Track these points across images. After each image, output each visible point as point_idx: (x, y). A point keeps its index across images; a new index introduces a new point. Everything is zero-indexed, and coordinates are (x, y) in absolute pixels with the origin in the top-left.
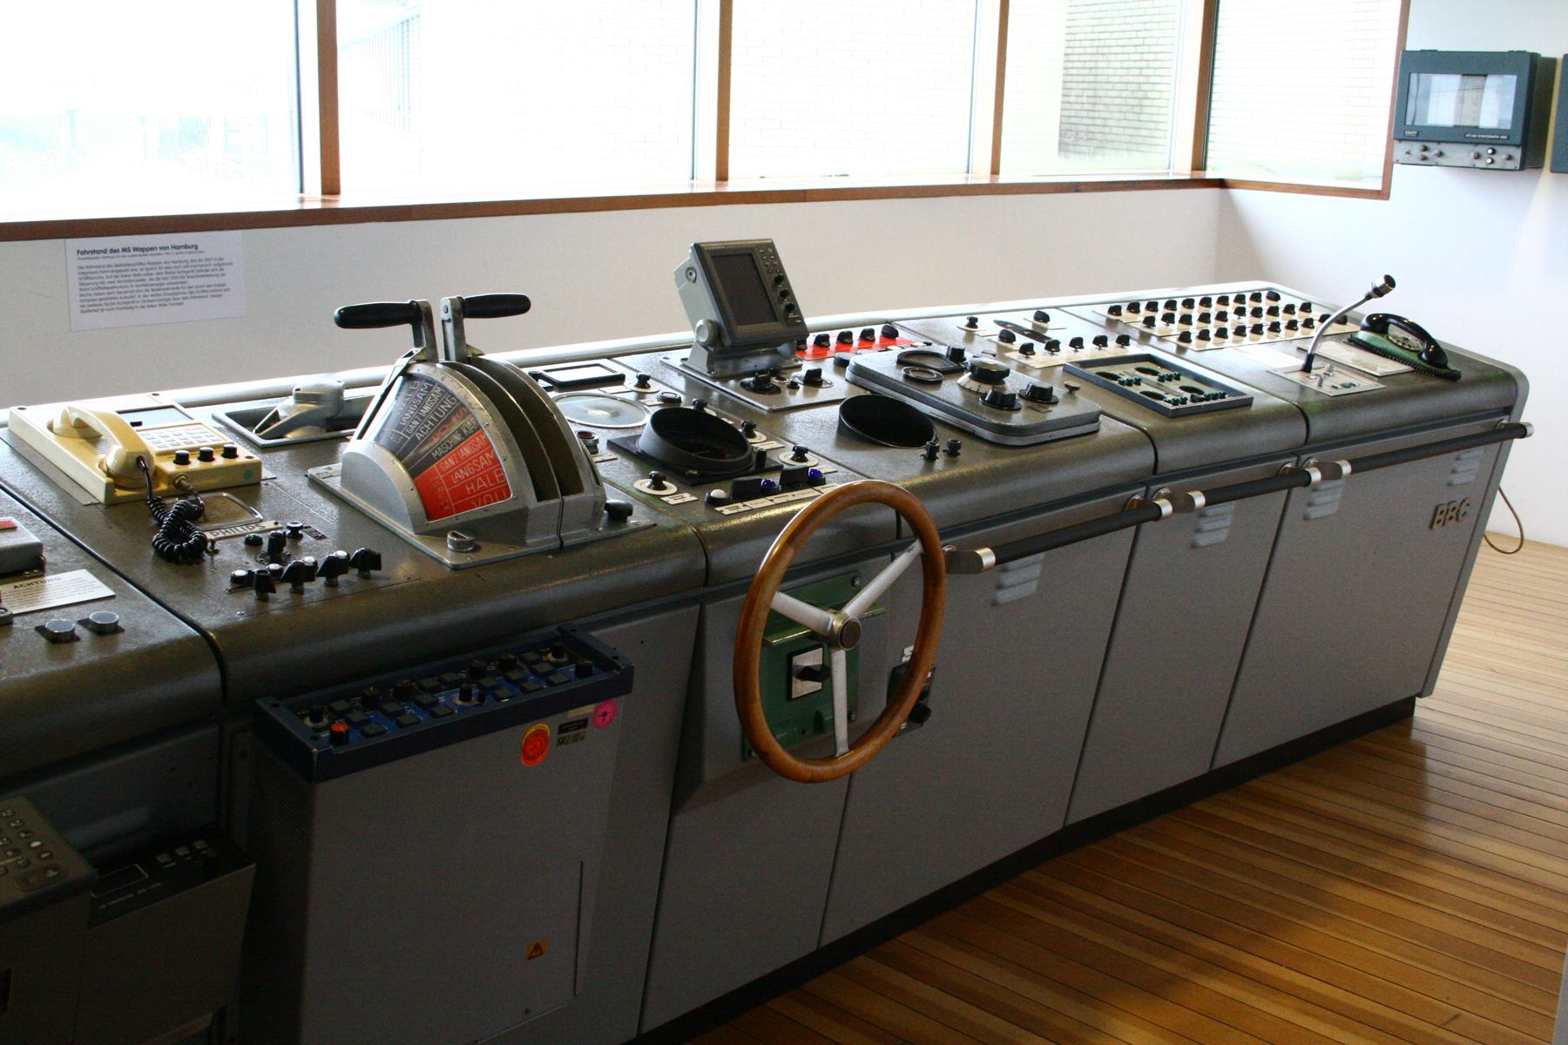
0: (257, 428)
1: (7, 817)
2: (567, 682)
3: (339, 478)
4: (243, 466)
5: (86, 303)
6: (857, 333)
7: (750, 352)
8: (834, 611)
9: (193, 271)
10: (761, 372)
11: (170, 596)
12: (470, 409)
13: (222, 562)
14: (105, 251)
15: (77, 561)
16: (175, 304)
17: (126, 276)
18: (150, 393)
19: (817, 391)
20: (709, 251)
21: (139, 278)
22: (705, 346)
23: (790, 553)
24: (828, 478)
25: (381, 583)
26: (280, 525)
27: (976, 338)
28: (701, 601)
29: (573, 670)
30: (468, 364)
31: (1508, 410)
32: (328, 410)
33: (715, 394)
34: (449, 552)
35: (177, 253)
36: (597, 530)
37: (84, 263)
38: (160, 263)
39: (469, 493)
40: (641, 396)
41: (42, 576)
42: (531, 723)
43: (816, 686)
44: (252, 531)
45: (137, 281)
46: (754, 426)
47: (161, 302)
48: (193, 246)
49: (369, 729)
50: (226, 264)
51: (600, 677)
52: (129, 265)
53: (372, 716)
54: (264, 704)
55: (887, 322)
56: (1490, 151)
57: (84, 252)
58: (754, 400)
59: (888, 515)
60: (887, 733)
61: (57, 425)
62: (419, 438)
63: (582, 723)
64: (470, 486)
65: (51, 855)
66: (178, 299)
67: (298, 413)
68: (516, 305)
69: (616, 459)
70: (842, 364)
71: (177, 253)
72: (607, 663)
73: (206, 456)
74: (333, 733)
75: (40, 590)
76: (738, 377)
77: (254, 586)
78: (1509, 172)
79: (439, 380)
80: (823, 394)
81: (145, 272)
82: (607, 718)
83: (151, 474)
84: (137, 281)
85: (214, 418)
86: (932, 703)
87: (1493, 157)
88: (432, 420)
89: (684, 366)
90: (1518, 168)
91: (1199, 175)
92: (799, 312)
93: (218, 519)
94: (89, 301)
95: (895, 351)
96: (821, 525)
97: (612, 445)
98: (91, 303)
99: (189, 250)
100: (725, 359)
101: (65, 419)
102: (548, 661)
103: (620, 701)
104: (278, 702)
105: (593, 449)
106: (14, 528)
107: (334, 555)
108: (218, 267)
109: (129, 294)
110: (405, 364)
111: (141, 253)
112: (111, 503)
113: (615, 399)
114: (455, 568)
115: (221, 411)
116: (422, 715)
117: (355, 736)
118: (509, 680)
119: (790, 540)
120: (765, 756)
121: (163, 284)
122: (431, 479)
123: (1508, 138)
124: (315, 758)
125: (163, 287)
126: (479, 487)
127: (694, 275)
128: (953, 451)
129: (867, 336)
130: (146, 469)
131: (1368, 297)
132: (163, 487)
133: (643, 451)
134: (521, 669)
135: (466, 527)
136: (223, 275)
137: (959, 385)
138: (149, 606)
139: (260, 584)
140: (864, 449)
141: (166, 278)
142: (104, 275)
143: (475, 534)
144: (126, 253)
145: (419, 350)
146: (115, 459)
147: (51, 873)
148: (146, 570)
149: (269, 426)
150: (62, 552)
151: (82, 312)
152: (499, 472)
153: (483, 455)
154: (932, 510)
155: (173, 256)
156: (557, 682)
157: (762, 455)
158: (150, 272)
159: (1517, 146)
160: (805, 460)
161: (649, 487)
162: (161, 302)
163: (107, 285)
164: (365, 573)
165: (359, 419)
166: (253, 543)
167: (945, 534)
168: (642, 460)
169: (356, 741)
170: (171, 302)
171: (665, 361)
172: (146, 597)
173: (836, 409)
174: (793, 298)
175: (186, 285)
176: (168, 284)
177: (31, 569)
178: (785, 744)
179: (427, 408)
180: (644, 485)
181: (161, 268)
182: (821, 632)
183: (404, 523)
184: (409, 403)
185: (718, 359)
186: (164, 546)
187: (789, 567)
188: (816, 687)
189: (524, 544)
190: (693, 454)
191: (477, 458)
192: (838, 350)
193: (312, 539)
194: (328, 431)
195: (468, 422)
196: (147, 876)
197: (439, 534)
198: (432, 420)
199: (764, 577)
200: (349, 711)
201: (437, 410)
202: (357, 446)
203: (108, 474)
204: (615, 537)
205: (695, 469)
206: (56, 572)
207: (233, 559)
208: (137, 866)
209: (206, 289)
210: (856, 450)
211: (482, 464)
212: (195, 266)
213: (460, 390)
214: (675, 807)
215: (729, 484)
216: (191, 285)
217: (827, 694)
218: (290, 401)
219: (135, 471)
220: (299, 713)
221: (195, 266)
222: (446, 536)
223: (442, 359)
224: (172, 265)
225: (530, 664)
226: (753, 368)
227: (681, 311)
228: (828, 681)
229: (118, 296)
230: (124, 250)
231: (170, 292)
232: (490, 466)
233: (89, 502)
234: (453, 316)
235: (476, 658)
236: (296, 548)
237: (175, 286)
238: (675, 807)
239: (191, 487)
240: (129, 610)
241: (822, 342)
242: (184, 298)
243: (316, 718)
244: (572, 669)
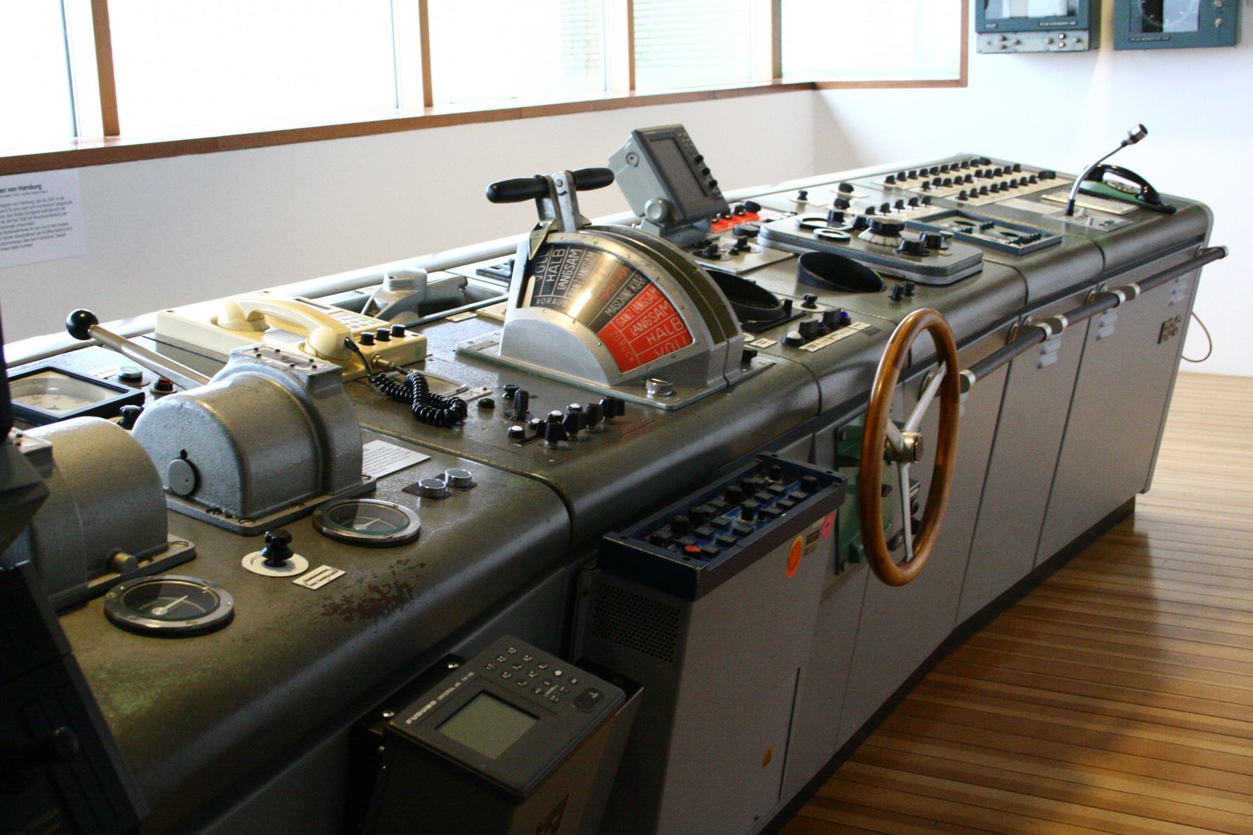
16: (25, 246)
27: (807, 206)
31: (1202, 237)
39: (651, 343)
42: (794, 537)
47: (14, 245)
48: (37, 187)
50: (67, 203)
56: (1062, 36)
61: (224, 320)
66: (28, 240)
71: (24, 194)
77: (546, 437)
78: (1079, 53)
87: (1065, 41)
90: (1087, 48)
91: (777, 81)
99: (34, 190)
123: (1077, 24)
125: (14, 229)
131: (1124, 144)
136: (65, 214)
141: (16, 220)
143: (672, 378)
155: (21, 197)
159: (1084, 30)
162: (14, 245)
181: (10, 210)
183: (596, 378)
189: (705, 386)
210: (835, 295)
212: (40, 206)
216: (38, 226)
220: (647, 538)
221: (40, 206)
224: (20, 206)
231: (20, 233)
232: (666, 317)
242: (34, 240)
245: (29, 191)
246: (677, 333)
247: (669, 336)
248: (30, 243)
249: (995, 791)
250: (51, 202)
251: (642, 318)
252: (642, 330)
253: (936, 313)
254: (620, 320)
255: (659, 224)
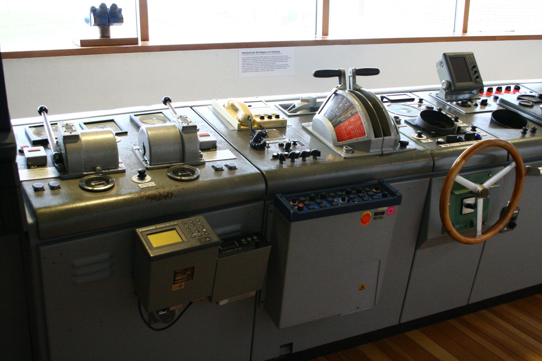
0: (288, 109)
1: (197, 221)
2: (378, 198)
3: (311, 127)
4: (281, 121)
5: (244, 69)
6: (504, 88)
7: (461, 92)
8: (480, 184)
9: (278, 60)
10: (465, 99)
11: (253, 160)
12: (355, 106)
13: (271, 151)
14: (250, 53)
15: (227, 147)
17: (256, 61)
18: (255, 97)
19: (485, 107)
20: (448, 56)
21: (261, 62)
22: (445, 90)
23: (464, 162)
24: (482, 137)
25: (320, 161)
26: (290, 140)
28: (431, 177)
29: (381, 195)
30: (356, 91)
32: (311, 105)
33: (448, 107)
34: (344, 153)
35: (273, 54)
36: (395, 149)
37: (244, 56)
38: (267, 57)
40: (420, 106)
41: (216, 151)
42: (365, 211)
43: (472, 211)
44: (281, 142)
45: (260, 63)
46: (458, 118)
47: (268, 70)
49: (310, 207)
50: (289, 58)
51: (390, 198)
52: (257, 57)
53: (312, 203)
54: (278, 196)
55: (517, 84)
57: (244, 53)
58: (461, 109)
59: (504, 152)
60: (497, 230)
61: (226, 105)
62: (337, 115)
63: (383, 213)
64: (353, 131)
65: (208, 234)
67: (301, 105)
68: (374, 72)
69: (406, 126)
70: (496, 98)
71: (273, 54)
72: (393, 194)
73: (270, 117)
74: (298, 207)
75: (215, 155)
76: (457, 101)
79: (346, 96)
80: (487, 108)
81: (263, 60)
82: (392, 212)
83: (252, 121)
84: (260, 63)
85: (275, 106)
86: (517, 222)
88: (342, 109)
89: (437, 96)
92: (481, 79)
93: (272, 137)
94: (245, 68)
95: (518, 94)
96: (476, 153)
97: (406, 122)
98: (245, 69)
99: (277, 53)
100: (452, 94)
101: (228, 104)
102: (373, 192)
103: (397, 207)
104: (282, 196)
105: (399, 122)
106: (209, 136)
107: (306, 151)
108: (286, 59)
109: (257, 67)
110: (335, 90)
111: (262, 53)
112: (239, 130)
113: (410, 106)
114: (345, 158)
115: (277, 104)
116: (328, 205)
117: (305, 209)
118: (358, 196)
119: (464, 158)
120: (449, 232)
121: (268, 64)
122: (340, 128)
124: (292, 214)
125: (268, 65)
126: (355, 132)
127: (442, 64)
128: (534, 131)
129: (508, 89)
130: (250, 120)
132: (256, 126)
133: (416, 124)
134: (363, 193)
135: (350, 145)
136: (287, 61)
137: (540, 108)
138: (246, 162)
139: (280, 158)
140: (499, 128)
142: (250, 60)
143: (354, 147)
144: (257, 54)
145: (340, 85)
146: (242, 116)
147: (208, 239)
148: (248, 152)
149: (292, 109)
150: (223, 144)
151: (243, 72)
152: (363, 127)
153: (358, 121)
154: (521, 152)
156: (375, 198)
157: (459, 128)
158: (264, 60)
160: (475, 131)
161: (417, 136)
163: (250, 64)
164: (315, 157)
165: (318, 108)
166: (281, 145)
167: (525, 161)
168: (415, 127)
169: (306, 210)
170: (270, 70)
171: (430, 94)
172: (246, 159)
173: (490, 114)
174: (479, 74)
175: (275, 64)
176: (270, 64)
177: (213, 148)
178: (457, 230)
179: (341, 105)
180: (415, 135)
181: (268, 59)
182: (474, 192)
183: (330, 142)
184: (335, 103)
185: (449, 95)
186: (253, 144)
187: (462, 168)
188: (472, 211)
189: (369, 152)
190: (434, 126)
191: (356, 122)
192: (496, 93)
193: (300, 145)
194: (311, 112)
195: (354, 111)
196: (238, 245)
197: (341, 147)
198: (342, 109)
199: (452, 170)
200: (305, 201)
201: (344, 106)
202: (319, 117)
203: (239, 121)
204: (401, 152)
205: (434, 131)
206: (220, 150)
207: (274, 149)
208: (235, 242)
209: (281, 66)
211: (357, 124)
212: (278, 58)
213: (352, 99)
214: (417, 248)
215: (445, 137)
216: (277, 64)
217: (475, 213)
218: (299, 101)
219: (247, 121)
221: (278, 58)
222: (343, 147)
223: (348, 88)
225: (367, 191)
226: (462, 98)
227: (438, 79)
228: (476, 209)
229: (254, 67)
230: (256, 52)
232: (360, 125)
233: (233, 129)
234: (353, 75)
235: (349, 188)
236: (294, 148)
237: (272, 64)
238: (417, 248)
239: (264, 127)
240: (240, 163)
241: (490, 90)
242: (274, 69)
243: (294, 201)
244: (381, 195)
245: (275, 53)
246: (362, 131)
247: (359, 132)
248: (273, 70)
249: (519, 332)
250: (283, 57)
251: (352, 124)
252: (350, 128)
253: (509, 140)
254: (345, 124)
255: (446, 90)
